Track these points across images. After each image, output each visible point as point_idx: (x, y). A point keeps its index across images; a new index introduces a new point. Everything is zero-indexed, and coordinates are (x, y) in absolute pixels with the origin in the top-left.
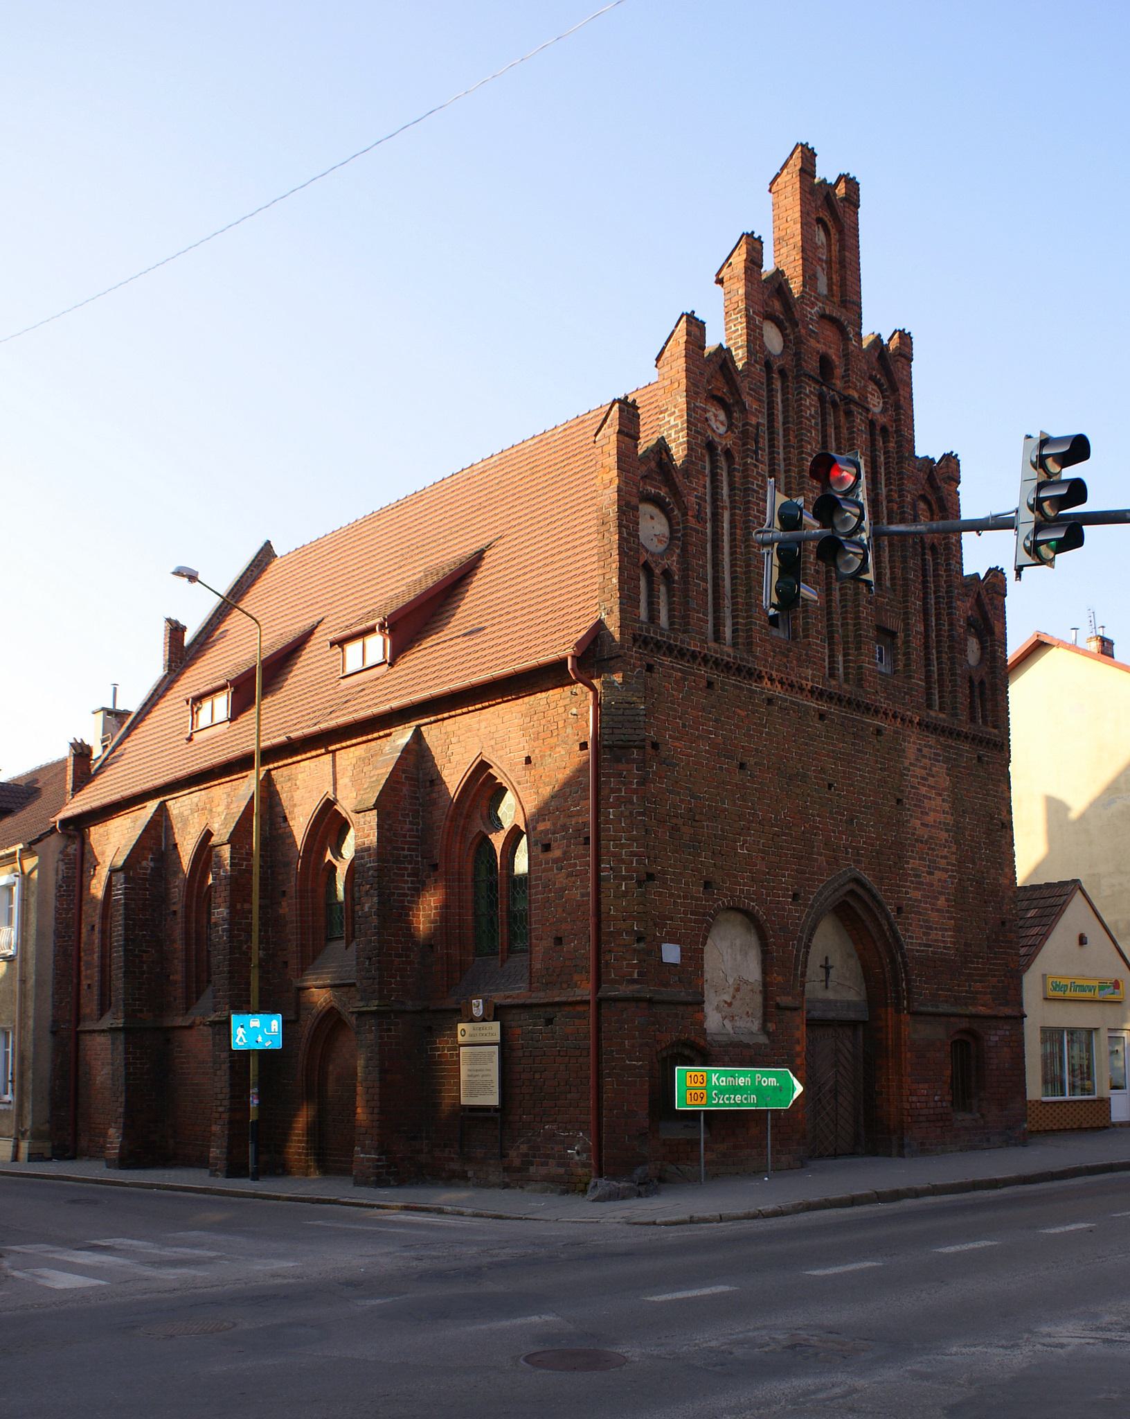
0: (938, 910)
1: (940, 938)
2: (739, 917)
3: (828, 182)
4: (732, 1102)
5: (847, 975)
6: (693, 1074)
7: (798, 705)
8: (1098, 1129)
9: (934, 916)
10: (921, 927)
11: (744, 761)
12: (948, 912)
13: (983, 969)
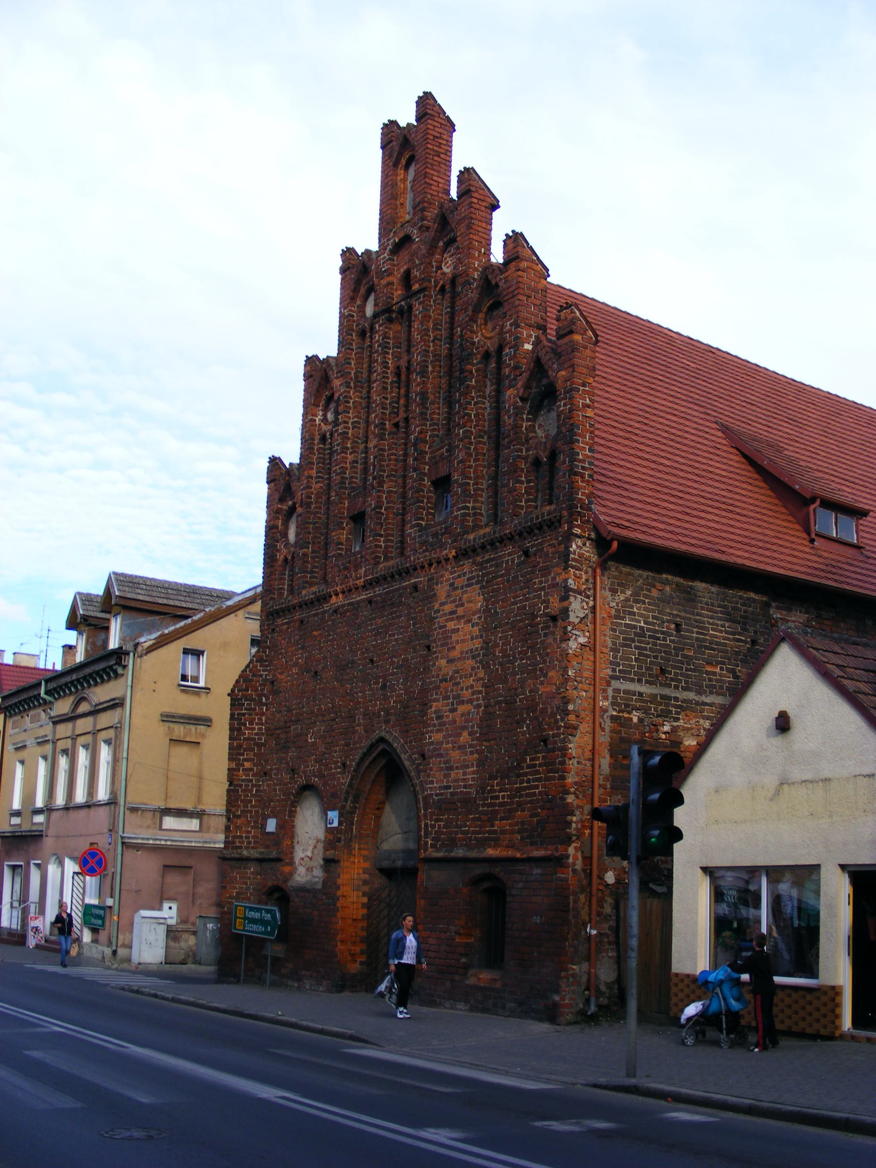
0: (460, 748)
1: (462, 777)
2: (307, 793)
3: (403, 124)
8: (816, 1037)
9: (455, 755)
10: (441, 769)
12: (471, 746)
13: (512, 803)
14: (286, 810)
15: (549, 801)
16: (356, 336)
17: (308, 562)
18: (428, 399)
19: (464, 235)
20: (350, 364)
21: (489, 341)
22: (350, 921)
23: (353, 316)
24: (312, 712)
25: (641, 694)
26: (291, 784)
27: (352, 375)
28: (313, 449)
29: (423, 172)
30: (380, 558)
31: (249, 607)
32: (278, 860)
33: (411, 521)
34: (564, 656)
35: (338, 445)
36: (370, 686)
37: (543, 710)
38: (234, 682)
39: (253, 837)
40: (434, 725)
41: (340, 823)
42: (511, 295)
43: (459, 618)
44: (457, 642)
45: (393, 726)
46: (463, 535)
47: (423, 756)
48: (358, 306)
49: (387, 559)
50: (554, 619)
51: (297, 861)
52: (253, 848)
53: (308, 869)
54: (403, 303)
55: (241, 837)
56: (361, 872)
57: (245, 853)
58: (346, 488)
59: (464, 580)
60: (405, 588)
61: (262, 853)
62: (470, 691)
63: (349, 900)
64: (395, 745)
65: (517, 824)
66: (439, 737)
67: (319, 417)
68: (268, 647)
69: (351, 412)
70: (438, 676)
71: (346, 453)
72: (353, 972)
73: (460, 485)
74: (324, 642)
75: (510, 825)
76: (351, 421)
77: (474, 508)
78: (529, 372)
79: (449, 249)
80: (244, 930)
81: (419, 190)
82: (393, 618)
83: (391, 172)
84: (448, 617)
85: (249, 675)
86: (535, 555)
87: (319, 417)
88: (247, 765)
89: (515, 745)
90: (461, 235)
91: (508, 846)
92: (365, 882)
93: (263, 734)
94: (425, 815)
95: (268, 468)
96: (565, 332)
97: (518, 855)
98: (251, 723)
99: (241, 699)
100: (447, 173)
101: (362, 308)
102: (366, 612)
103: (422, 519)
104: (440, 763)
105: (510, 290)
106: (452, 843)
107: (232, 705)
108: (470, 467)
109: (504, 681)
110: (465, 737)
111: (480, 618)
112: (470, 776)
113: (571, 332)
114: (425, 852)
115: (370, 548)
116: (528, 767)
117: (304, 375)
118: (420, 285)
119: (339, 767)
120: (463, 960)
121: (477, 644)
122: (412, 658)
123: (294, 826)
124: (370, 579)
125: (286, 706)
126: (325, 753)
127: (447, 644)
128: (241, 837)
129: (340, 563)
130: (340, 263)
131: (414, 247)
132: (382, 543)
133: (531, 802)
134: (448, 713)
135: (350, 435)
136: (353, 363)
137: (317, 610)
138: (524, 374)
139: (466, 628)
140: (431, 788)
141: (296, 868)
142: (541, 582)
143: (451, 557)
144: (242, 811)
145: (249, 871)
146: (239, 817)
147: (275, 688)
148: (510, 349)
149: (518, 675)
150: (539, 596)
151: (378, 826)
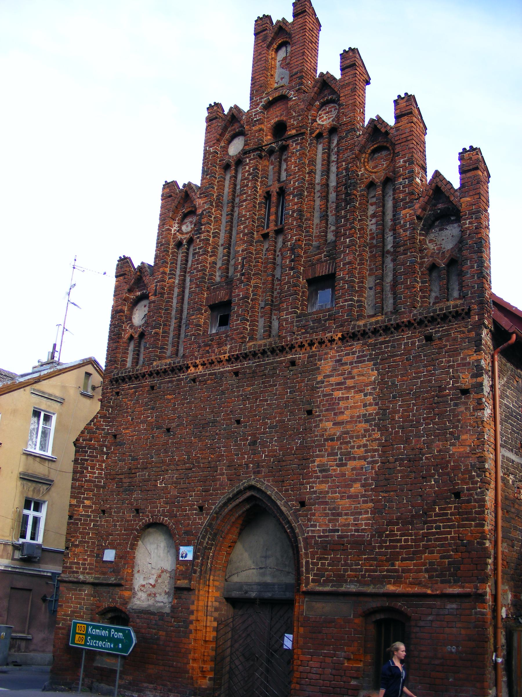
2: (150, 530)
4: (97, 645)
5: (287, 563)
6: (80, 625)
7: (215, 374)
11: (169, 427)
12: (363, 496)
14: (127, 543)
15: (463, 545)
16: (219, 168)
17: (159, 340)
18: (304, 216)
19: (349, 96)
20: (214, 188)
21: (374, 174)
22: (202, 642)
23: (217, 154)
24: (163, 462)
25: (513, 461)
26: (135, 521)
27: (215, 197)
28: (168, 252)
29: (302, 51)
30: (246, 338)
31: (34, 385)
32: (119, 585)
33: (287, 309)
34: (479, 423)
35: (199, 248)
36: (236, 441)
37: (456, 468)
38: (79, 433)
39: (89, 564)
40: (318, 477)
41: (195, 557)
42: (404, 140)
43: (349, 388)
44: (346, 408)
45: (265, 476)
46: (351, 322)
47: (303, 504)
48: (221, 147)
49: (252, 339)
50: (465, 392)
51: (137, 588)
52: (88, 573)
53: (149, 595)
54: (273, 145)
55: (78, 563)
56: (214, 600)
57: (81, 577)
58: (205, 283)
59: (354, 357)
60: (281, 362)
61: (96, 578)
62: (362, 449)
63: (202, 624)
64: (269, 493)
65: (424, 564)
66: (325, 487)
67: (175, 228)
68: (112, 407)
69: (212, 224)
70: (323, 435)
71: (207, 255)
72: (203, 687)
73: (346, 282)
74: (178, 404)
75: (415, 565)
76: (212, 231)
77: (358, 301)
78: (427, 197)
79: (324, 108)
80: (85, 645)
81: (296, 64)
82: (266, 387)
83: (265, 51)
84: (334, 387)
85: (92, 428)
86: (440, 339)
87: (175, 228)
88: (87, 502)
89: (421, 496)
90: (344, 96)
91: (411, 583)
92: (216, 609)
93: (102, 478)
94: (306, 554)
95: (118, 265)
96: (471, 167)
97: (429, 592)
98: (93, 468)
99: (85, 447)
100: (316, 57)
101: (225, 149)
102: (233, 381)
103: (298, 309)
104: (325, 509)
105: (404, 136)
106: (341, 579)
107: (77, 452)
108: (356, 268)
109: (407, 441)
110: (356, 488)
111: (374, 389)
112: (363, 522)
113: (477, 168)
114: (306, 586)
115: (237, 329)
116: (436, 515)
117: (162, 196)
118: (297, 131)
119: (196, 510)
120: (353, 682)
121: (372, 410)
122: (289, 420)
123: (134, 557)
124: (237, 355)
125: (130, 456)
126: (178, 497)
127: (334, 409)
128: (78, 563)
129: (200, 341)
130: (206, 114)
131: (290, 103)
132: (248, 327)
133: (442, 546)
134: (335, 467)
135: (210, 242)
136: (216, 188)
137: (172, 378)
138: (421, 199)
139: (357, 397)
140: (313, 531)
141: (135, 593)
142: (449, 361)
143: (336, 338)
144: (80, 542)
145: (83, 593)
146: (77, 546)
147: (118, 440)
148: (403, 179)
149: (424, 437)
150: (448, 373)
151: (228, 562)
